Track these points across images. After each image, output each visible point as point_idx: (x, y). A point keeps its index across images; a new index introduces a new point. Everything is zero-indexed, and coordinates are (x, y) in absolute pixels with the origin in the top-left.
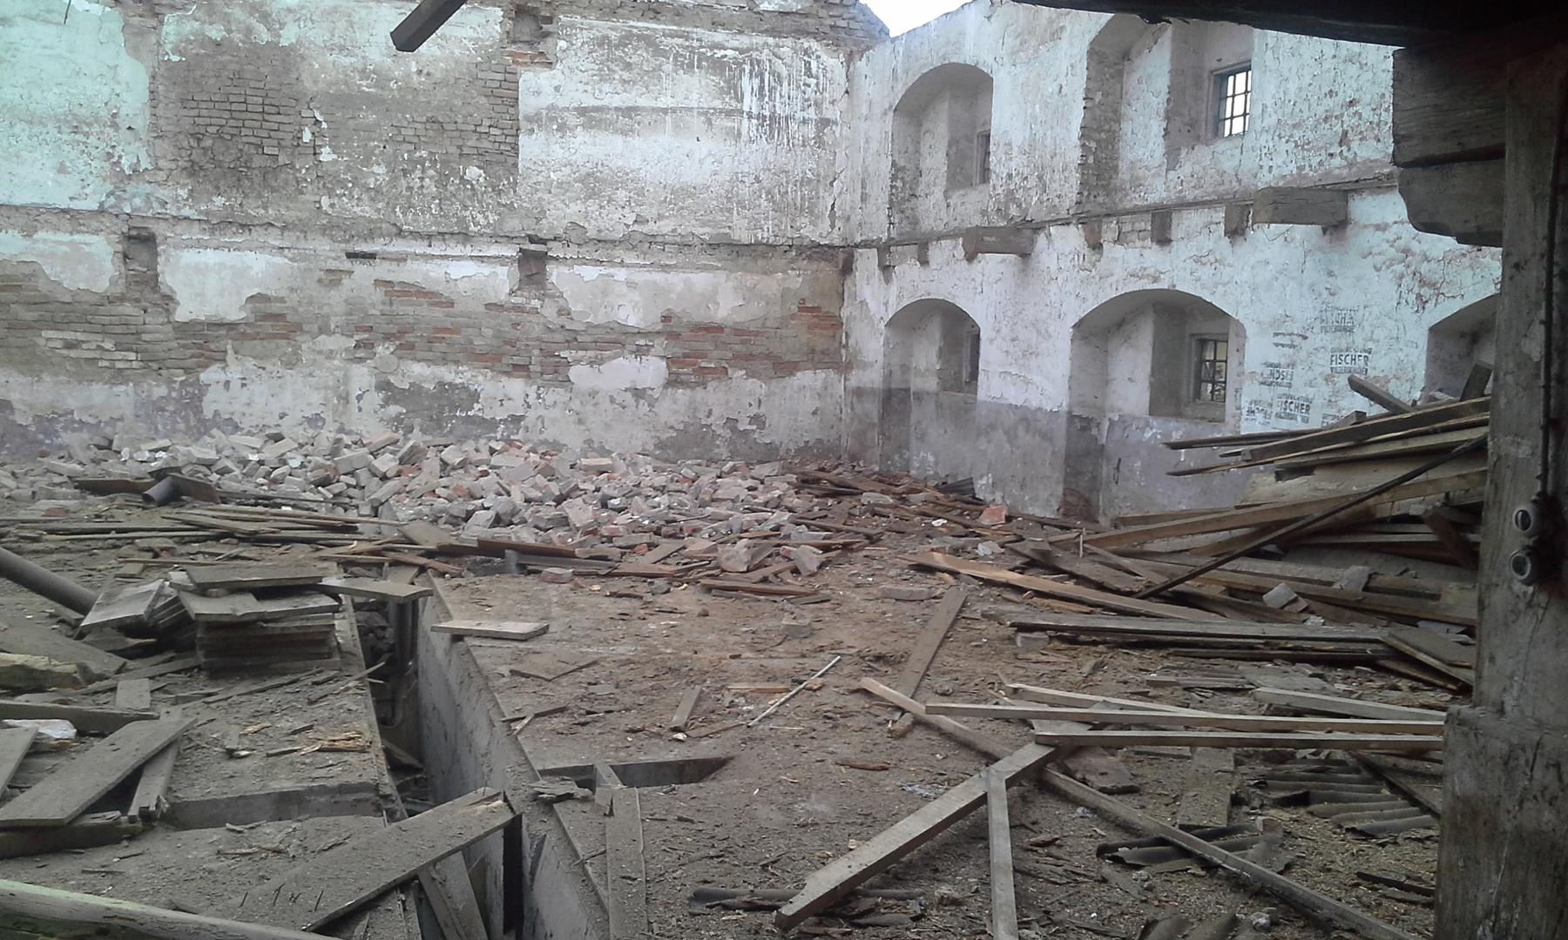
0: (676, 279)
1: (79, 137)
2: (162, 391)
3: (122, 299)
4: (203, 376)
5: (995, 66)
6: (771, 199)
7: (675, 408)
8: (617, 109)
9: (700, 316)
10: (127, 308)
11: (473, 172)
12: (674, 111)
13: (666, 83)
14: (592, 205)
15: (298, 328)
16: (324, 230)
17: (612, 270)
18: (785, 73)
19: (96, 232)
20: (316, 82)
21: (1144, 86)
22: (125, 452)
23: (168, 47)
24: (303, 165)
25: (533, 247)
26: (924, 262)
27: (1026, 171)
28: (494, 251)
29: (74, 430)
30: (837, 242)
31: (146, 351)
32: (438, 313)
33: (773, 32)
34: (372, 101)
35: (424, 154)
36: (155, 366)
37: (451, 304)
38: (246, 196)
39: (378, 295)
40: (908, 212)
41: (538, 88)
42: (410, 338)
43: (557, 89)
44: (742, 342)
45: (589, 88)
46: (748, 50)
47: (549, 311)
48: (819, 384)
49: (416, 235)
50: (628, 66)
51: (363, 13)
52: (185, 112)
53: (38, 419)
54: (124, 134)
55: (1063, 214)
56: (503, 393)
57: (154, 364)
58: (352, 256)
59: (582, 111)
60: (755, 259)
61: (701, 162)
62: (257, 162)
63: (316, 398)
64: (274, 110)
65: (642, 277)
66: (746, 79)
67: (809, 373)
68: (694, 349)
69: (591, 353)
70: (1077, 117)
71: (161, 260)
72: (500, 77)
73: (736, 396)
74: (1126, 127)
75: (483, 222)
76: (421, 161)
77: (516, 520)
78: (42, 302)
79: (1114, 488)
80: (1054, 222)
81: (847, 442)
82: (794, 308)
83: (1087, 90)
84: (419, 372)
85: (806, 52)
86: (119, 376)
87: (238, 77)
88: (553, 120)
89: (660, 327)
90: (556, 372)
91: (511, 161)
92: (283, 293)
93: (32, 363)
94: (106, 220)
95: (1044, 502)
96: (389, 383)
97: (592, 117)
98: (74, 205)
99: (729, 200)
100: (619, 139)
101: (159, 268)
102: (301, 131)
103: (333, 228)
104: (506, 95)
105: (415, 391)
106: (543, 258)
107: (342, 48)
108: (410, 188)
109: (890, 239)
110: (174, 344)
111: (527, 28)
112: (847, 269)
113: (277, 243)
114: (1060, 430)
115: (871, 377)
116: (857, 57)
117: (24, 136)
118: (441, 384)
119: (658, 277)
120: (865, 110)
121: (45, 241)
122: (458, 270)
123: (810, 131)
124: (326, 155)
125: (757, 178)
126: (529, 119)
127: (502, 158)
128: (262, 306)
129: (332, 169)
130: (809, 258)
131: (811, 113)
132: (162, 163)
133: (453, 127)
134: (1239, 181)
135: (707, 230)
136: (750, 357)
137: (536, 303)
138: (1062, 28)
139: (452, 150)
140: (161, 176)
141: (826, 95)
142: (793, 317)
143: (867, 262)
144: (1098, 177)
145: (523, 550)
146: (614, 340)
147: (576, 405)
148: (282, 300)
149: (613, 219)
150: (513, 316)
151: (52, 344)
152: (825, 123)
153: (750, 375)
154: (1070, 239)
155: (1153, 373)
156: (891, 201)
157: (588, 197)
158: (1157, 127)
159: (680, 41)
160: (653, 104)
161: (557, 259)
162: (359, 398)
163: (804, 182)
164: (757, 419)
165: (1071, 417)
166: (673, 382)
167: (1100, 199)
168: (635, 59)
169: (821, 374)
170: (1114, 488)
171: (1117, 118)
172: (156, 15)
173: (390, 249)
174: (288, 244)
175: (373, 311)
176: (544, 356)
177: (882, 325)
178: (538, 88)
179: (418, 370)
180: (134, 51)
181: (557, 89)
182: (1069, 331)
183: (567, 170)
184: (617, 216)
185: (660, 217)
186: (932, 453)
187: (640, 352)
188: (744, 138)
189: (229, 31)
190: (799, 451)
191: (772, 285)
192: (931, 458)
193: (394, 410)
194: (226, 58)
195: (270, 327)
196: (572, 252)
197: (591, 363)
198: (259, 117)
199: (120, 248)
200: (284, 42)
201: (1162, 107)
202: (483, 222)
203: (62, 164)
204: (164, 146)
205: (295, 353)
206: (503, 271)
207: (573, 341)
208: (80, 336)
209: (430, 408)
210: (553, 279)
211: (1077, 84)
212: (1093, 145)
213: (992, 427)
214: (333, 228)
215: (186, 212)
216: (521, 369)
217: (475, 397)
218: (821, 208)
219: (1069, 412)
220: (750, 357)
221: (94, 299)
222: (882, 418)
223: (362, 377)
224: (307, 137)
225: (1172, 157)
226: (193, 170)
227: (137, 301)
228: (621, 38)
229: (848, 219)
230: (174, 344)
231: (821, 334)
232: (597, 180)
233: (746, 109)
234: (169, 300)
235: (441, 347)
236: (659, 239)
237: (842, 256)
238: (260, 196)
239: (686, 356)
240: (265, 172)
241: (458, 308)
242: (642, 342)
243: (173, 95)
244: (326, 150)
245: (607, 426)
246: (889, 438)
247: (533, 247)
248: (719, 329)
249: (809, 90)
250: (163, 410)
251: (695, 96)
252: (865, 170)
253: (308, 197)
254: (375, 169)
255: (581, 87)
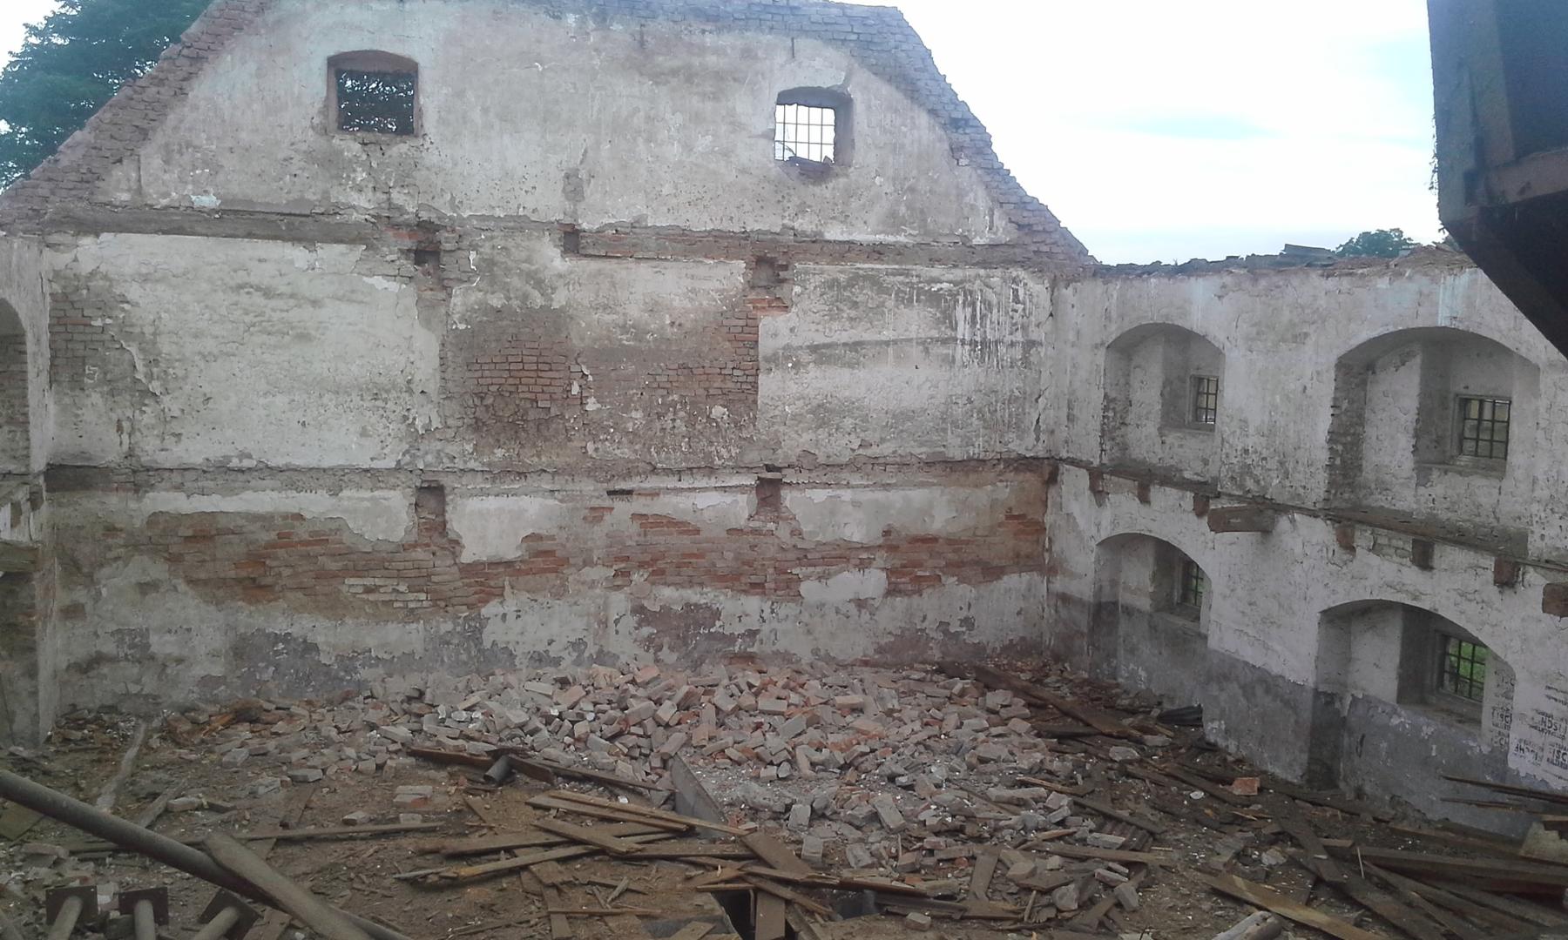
0: (895, 497)
1: (379, 403)
2: (447, 626)
3: (415, 546)
4: (483, 611)
5: (1228, 344)
6: (982, 418)
7: (892, 616)
8: (845, 344)
9: (917, 530)
10: (419, 554)
11: (718, 411)
12: (895, 342)
13: (889, 317)
14: (822, 434)
15: (565, 562)
16: (590, 473)
17: (838, 492)
18: (994, 300)
19: (394, 487)
20: (582, 339)
21: (1390, 400)
22: (442, 711)
23: (456, 317)
24: (571, 415)
25: (770, 475)
26: (1144, 499)
27: (1265, 453)
28: (735, 481)
29: (371, 666)
30: (1041, 454)
31: (435, 591)
32: (686, 540)
33: (984, 264)
34: (631, 353)
35: (676, 397)
36: (442, 604)
37: (698, 531)
38: (522, 446)
39: (635, 528)
40: (1118, 440)
41: (775, 330)
42: (661, 564)
43: (792, 330)
44: (954, 551)
45: (820, 327)
46: (962, 282)
47: (783, 532)
48: (1024, 586)
49: (668, 472)
50: (855, 305)
51: (624, 273)
52: (469, 374)
53: (340, 658)
54: (418, 397)
55: (1309, 505)
56: (740, 611)
57: (442, 602)
58: (610, 493)
59: (814, 349)
60: (967, 474)
61: (919, 387)
62: (532, 415)
63: (579, 624)
64: (546, 367)
65: (868, 496)
66: (959, 308)
67: (1015, 577)
68: (911, 559)
69: (819, 569)
70: (1324, 422)
71: (449, 508)
72: (742, 323)
73: (945, 603)
74: (1371, 432)
75: (726, 455)
76: (673, 404)
77: (828, 813)
78: (348, 553)
79: (1356, 760)
80: (1301, 510)
81: (1050, 641)
82: (1002, 517)
83: (1335, 399)
84: (670, 595)
85: (1014, 281)
86: (412, 615)
87: (516, 338)
88: (787, 358)
89: (880, 541)
90: (788, 587)
91: (751, 398)
92: (554, 531)
93: (335, 607)
94: (402, 477)
95: (1288, 766)
96: (643, 607)
97: (822, 354)
98: (375, 465)
99: (944, 420)
100: (846, 372)
101: (447, 516)
102: (570, 384)
103: (596, 470)
104: (747, 338)
105: (666, 611)
106: (777, 484)
107: (605, 307)
108: (663, 430)
109: (1102, 464)
110: (459, 584)
111: (765, 274)
112: (1052, 479)
113: (549, 487)
114: (1307, 699)
115: (1083, 589)
116: (1062, 284)
117: (332, 405)
118: (688, 605)
119: (880, 495)
120: (1071, 336)
121: (349, 498)
122: (706, 501)
123: (1017, 353)
124: (592, 405)
125: (970, 401)
126: (767, 360)
127: (744, 396)
128: (534, 544)
129: (597, 417)
130: (1016, 470)
131: (1019, 337)
132: (450, 422)
133: (701, 371)
134: (1498, 520)
135: (923, 449)
136: (960, 564)
137: (771, 526)
138: (1306, 335)
139: (701, 392)
140: (450, 433)
141: (1032, 318)
142: (1000, 525)
143: (1074, 482)
144: (1345, 476)
145: (881, 891)
146: (843, 555)
147: (805, 617)
148: (552, 538)
149: (840, 446)
150: (751, 538)
151: (353, 590)
152: (1030, 344)
153: (961, 581)
154: (1320, 532)
155: (1401, 665)
156: (1103, 430)
157: (818, 427)
158: (1405, 442)
159: (901, 278)
160: (877, 337)
161: (790, 484)
162: (617, 622)
163: (1011, 400)
164: (968, 622)
165: (1317, 693)
166: (892, 591)
167: (1346, 496)
168: (861, 298)
169: (1026, 577)
170: (1356, 760)
171: (1360, 420)
172: (445, 288)
173: (646, 485)
174: (557, 487)
175: (629, 543)
176: (773, 572)
177: (1093, 544)
178: (775, 330)
179: (668, 593)
180: (427, 323)
181: (792, 330)
182: (1316, 617)
183: (800, 403)
184: (844, 442)
185: (883, 440)
186: (1141, 668)
187: (863, 565)
188: (959, 363)
189: (508, 299)
190: (1005, 649)
191: (982, 497)
192: (1143, 674)
193: (646, 631)
194: (505, 323)
195: (543, 562)
196: (803, 478)
197: (819, 579)
198: (533, 374)
199: (413, 500)
200: (556, 306)
201: (1411, 426)
202: (726, 455)
203: (364, 428)
204: (453, 407)
205: (563, 585)
206: (742, 499)
207: (803, 558)
208: (378, 582)
209: (678, 627)
210: (787, 503)
211: (1325, 390)
212: (1340, 448)
213: (1226, 678)
214: (596, 470)
215: (472, 464)
216: (757, 587)
217: (716, 615)
218: (1027, 422)
219: (1316, 690)
220: (960, 564)
221: (391, 548)
222: (1092, 630)
223: (619, 602)
224: (575, 390)
225: (1423, 472)
226: (478, 426)
227: (428, 545)
228: (851, 279)
229: (1052, 432)
230: (459, 584)
231: (1028, 541)
232: (827, 410)
233: (960, 336)
234: (455, 544)
235: (686, 571)
236: (881, 461)
237: (1047, 470)
238: (534, 446)
239: (904, 566)
240: (539, 424)
241: (703, 535)
242: (864, 556)
243: (459, 360)
244: (592, 400)
245: (832, 635)
246: (1098, 649)
247: (770, 475)
248: (934, 540)
249: (1016, 315)
250: (448, 643)
251: (914, 328)
252: (1073, 392)
253: (577, 444)
254: (634, 414)
255: (814, 327)
